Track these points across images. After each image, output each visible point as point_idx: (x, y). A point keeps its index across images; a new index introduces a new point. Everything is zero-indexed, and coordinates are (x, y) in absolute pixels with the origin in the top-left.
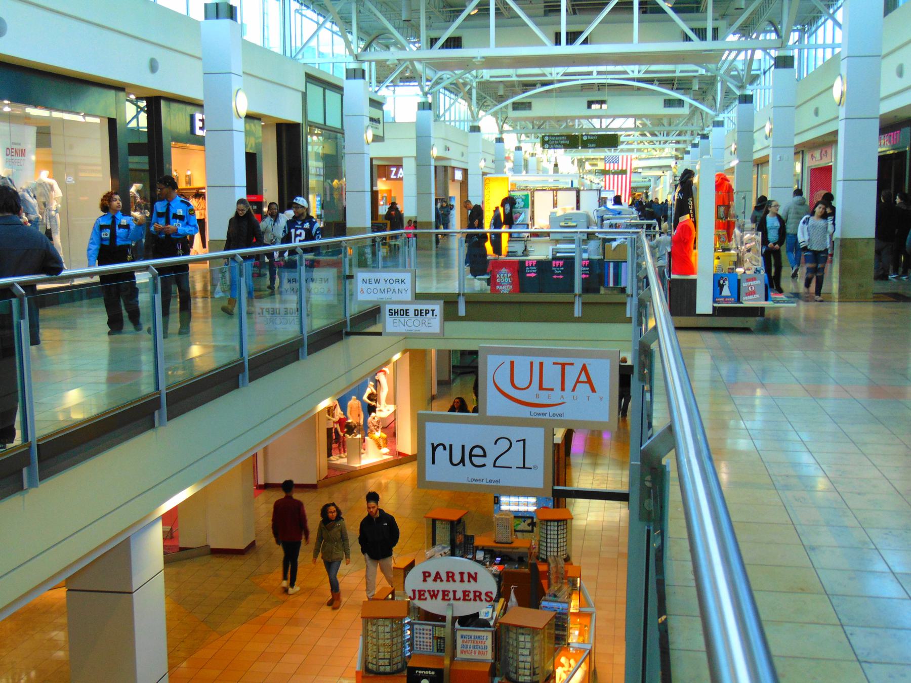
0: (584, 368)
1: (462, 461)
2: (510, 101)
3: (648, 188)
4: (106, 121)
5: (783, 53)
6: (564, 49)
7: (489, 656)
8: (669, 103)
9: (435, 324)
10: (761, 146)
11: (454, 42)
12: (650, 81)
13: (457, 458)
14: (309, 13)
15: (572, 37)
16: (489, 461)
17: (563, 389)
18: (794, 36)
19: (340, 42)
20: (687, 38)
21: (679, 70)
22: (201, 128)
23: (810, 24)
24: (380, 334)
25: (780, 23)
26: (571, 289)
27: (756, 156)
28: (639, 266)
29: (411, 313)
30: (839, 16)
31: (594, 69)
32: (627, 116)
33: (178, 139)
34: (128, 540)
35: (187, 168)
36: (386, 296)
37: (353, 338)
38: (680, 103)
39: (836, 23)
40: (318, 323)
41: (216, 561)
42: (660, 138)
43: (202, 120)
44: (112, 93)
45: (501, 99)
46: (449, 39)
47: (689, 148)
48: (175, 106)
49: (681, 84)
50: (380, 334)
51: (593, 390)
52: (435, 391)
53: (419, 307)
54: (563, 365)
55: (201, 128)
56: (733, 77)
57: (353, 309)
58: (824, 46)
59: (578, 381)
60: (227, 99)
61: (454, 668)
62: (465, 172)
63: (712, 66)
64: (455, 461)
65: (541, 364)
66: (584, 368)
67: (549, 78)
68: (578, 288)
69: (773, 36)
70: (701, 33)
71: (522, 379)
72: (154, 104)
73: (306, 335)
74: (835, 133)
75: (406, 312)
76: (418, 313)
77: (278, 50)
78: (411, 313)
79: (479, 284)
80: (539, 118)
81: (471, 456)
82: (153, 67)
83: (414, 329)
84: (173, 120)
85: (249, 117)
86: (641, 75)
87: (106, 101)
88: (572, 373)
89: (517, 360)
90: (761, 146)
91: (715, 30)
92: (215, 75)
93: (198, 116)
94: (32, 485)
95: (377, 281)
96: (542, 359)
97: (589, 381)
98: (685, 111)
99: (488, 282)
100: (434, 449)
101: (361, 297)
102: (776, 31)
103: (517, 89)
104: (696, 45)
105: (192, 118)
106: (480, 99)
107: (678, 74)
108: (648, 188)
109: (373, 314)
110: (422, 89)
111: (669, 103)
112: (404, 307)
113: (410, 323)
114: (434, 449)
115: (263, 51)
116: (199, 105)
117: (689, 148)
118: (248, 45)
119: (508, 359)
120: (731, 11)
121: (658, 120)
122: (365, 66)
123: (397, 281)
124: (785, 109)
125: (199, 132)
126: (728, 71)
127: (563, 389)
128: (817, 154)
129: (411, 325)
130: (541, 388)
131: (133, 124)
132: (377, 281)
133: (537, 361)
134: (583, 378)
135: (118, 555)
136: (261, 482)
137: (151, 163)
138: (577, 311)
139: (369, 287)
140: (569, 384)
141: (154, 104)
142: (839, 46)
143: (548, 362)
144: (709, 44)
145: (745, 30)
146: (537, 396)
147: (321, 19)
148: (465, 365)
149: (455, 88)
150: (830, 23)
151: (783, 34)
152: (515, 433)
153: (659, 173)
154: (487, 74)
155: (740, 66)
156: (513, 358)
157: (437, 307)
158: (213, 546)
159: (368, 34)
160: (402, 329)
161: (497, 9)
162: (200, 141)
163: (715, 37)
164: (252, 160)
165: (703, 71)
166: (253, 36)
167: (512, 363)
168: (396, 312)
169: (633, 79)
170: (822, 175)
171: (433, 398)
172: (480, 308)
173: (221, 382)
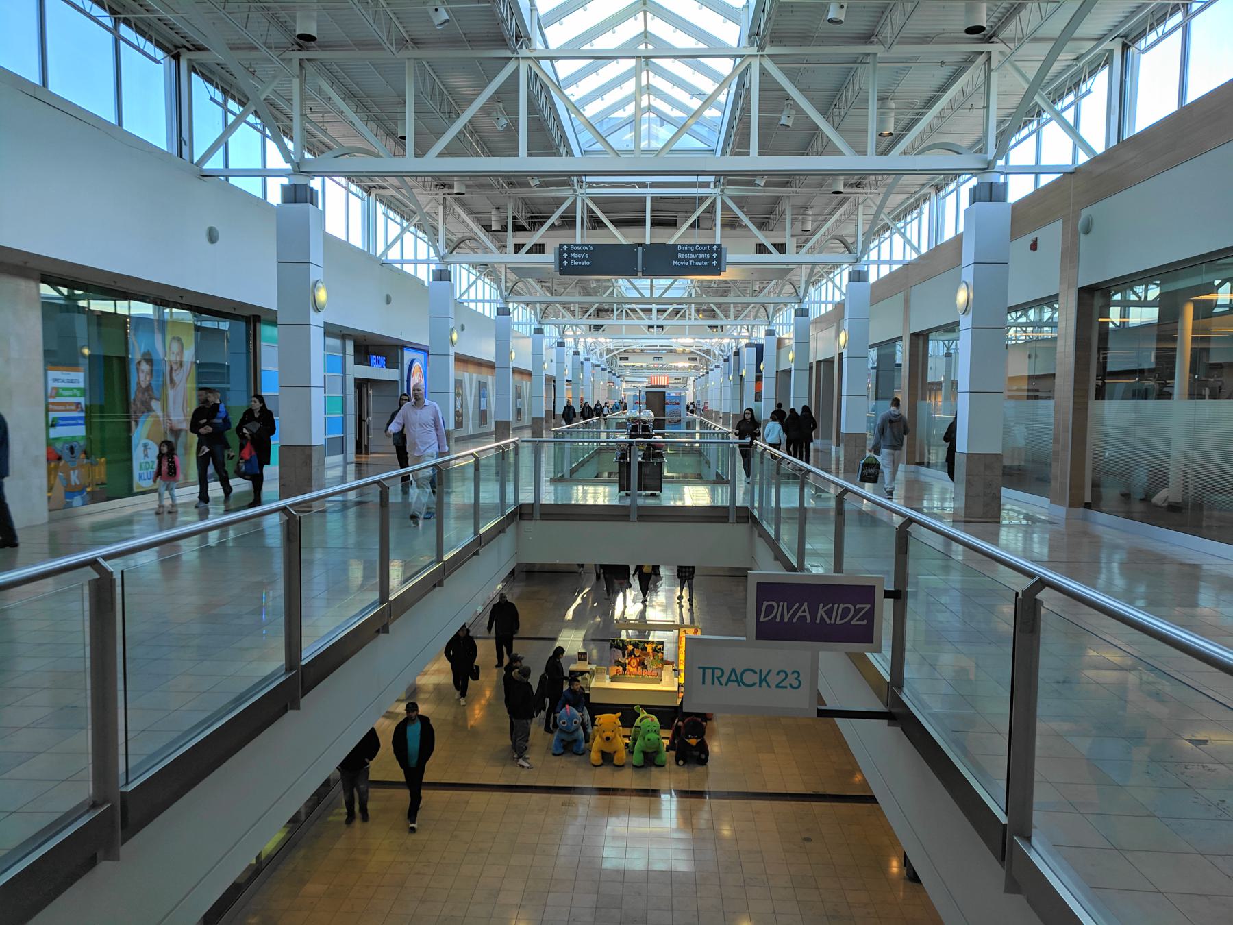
29: (654, 312)
75: (650, 310)
92: (293, 264)
115: (345, 246)
147: (405, 224)
150: (830, 284)
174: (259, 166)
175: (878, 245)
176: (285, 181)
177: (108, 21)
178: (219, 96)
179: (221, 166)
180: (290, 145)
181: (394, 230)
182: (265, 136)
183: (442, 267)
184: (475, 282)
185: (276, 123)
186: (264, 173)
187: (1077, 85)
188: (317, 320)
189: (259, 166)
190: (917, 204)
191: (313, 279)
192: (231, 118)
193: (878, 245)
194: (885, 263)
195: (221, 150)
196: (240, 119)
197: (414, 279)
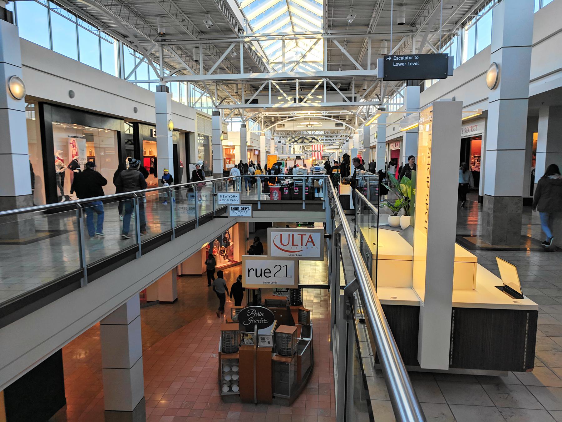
0: (310, 236)
1: (261, 275)
2: (276, 124)
3: (328, 157)
4: (116, 132)
5: (381, 107)
6: (298, 104)
7: (271, 345)
8: (337, 125)
9: (249, 213)
10: (373, 141)
11: (255, 101)
12: (330, 116)
13: (258, 274)
14: (198, 89)
15: (301, 100)
16: (272, 275)
17: (302, 245)
18: (385, 100)
19: (210, 100)
20: (344, 101)
21: (341, 112)
22: (155, 135)
23: (391, 95)
24: (227, 217)
25: (380, 95)
26: (302, 199)
27: (371, 145)
28: (329, 192)
29: (240, 209)
30: (402, 93)
31: (309, 112)
32: (321, 130)
33: (145, 139)
34: (126, 303)
35: (149, 150)
36: (229, 202)
37: (217, 219)
38: (342, 125)
39: (401, 95)
40: (204, 213)
41: (161, 306)
42: (334, 138)
43: (155, 132)
44: (119, 120)
45: (273, 123)
46: (253, 100)
47: (345, 142)
48: (144, 125)
49: (343, 118)
50: (227, 217)
51: (314, 245)
52: (248, 237)
53: (243, 207)
54: (302, 235)
55: (155, 135)
56: (362, 115)
57: (217, 207)
58: (396, 104)
59: (308, 242)
60: (166, 122)
61: (258, 350)
62: (259, 151)
63: (354, 111)
64: (258, 275)
65: (293, 235)
66: (310, 236)
67: (292, 115)
68: (304, 198)
69: (377, 100)
70: (350, 99)
71: (285, 241)
72: (136, 125)
73: (198, 218)
74: (402, 137)
75: (238, 209)
76: (242, 209)
77: (186, 104)
78: (240, 209)
79: (265, 197)
80: (287, 131)
81: (264, 273)
82: (135, 110)
83: (241, 215)
84: (144, 131)
85: (175, 130)
86: (327, 114)
87: (116, 125)
88: (305, 239)
89: (283, 233)
90: (373, 141)
91: (355, 98)
92: (161, 114)
93: (154, 130)
94: (85, 285)
95: (226, 197)
96: (293, 233)
97: (312, 242)
98: (344, 128)
99: (269, 196)
100: (249, 271)
101: (220, 203)
102: (378, 98)
103: (280, 119)
104: (348, 103)
105: (151, 130)
106: (265, 122)
107: (341, 114)
108: (328, 157)
109: (225, 209)
110: (242, 119)
111: (337, 125)
112: (237, 207)
113: (239, 213)
114: (249, 271)
115: (180, 104)
116: (154, 125)
117: (345, 142)
118: (173, 102)
119: (279, 233)
120: (361, 90)
121: (333, 132)
122: (220, 110)
123: (234, 196)
124: (382, 127)
125: (154, 136)
126: (360, 112)
127: (302, 245)
128: (394, 144)
129: (240, 213)
130: (293, 245)
131: (128, 132)
132: (226, 197)
133: (291, 234)
134: (310, 240)
135: (123, 309)
136: (180, 274)
137: (134, 147)
138: (304, 207)
139: (223, 199)
140: (304, 243)
141: (136, 125)
142: (402, 104)
143: (296, 234)
144: (353, 103)
145: (366, 97)
146: (291, 248)
147: (203, 92)
148: (261, 228)
149: (255, 119)
150: (398, 95)
151: (381, 99)
152: (283, 263)
153: (333, 151)
154: (267, 114)
155: (365, 111)
156: (281, 233)
157: (250, 207)
158: (160, 301)
159: (221, 97)
160: (236, 215)
161: (272, 89)
162: (155, 140)
163: (355, 101)
164: (175, 147)
165: (350, 113)
166: (176, 98)
167: (281, 235)
168: (234, 209)
169: (323, 116)
170: (396, 153)
171: (248, 239)
172: (266, 206)
173: (165, 238)
174: (147, 79)
175: (476, 22)
176: (158, 84)
177: (97, 33)
178: (133, 52)
179: (134, 79)
180: (157, 66)
181: (198, 95)
182: (100, 37)
183: (161, 84)
184: (200, 98)
185: (152, 58)
186: (149, 82)
187: (477, 14)
188: (247, 148)
189: (147, 79)
190: (450, 38)
191: (168, 119)
192: (138, 61)
193: (476, 22)
194: (398, 104)
195: (134, 74)
196: (142, 60)
197: (149, 91)
